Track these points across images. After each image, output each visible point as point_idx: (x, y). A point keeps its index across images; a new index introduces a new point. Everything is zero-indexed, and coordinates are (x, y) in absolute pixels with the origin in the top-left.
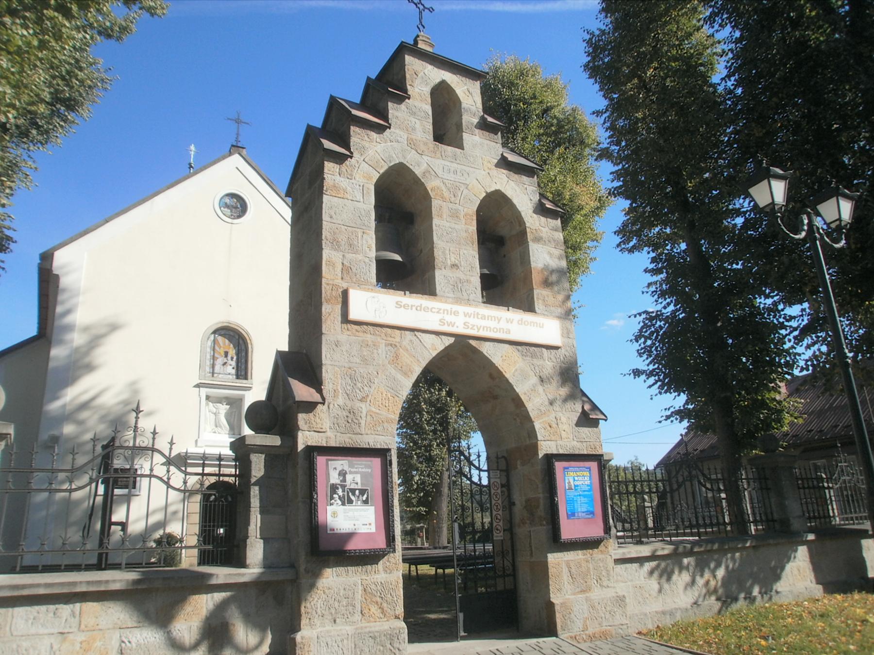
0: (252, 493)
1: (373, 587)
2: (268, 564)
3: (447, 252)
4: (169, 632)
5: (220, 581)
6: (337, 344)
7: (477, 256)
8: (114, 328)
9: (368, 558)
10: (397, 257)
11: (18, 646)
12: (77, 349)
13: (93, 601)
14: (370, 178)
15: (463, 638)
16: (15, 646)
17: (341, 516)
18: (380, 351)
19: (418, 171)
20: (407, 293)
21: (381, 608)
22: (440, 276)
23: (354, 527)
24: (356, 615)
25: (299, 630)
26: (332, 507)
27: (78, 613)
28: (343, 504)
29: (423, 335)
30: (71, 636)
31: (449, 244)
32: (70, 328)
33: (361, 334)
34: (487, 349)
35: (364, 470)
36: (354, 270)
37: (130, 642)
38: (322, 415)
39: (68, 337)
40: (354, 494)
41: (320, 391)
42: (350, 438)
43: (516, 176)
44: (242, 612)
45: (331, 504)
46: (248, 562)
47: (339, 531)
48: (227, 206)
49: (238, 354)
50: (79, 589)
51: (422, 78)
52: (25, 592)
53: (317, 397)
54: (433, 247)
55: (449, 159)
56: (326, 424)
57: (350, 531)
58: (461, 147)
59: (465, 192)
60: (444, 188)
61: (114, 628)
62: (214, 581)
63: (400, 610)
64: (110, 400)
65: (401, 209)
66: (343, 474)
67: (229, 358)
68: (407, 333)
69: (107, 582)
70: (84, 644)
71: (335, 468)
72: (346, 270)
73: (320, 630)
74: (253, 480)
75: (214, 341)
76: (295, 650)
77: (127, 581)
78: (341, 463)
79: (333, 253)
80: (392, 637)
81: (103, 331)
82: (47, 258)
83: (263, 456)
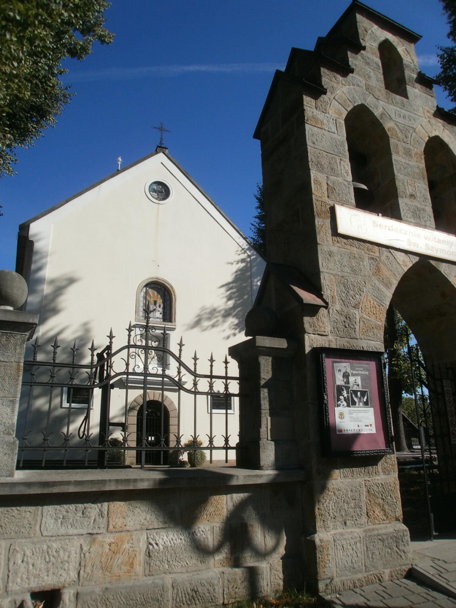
0: (262, 396)
1: (375, 488)
2: (278, 465)
3: (406, 183)
4: (194, 534)
5: (241, 482)
6: (331, 254)
7: (428, 189)
8: (71, 281)
9: (370, 460)
10: (364, 187)
11: (48, 547)
12: (46, 297)
13: (121, 501)
14: (340, 114)
15: (436, 537)
16: (45, 547)
17: (347, 416)
18: (365, 263)
19: (377, 113)
20: (380, 215)
21: (383, 510)
22: (402, 202)
23: (357, 428)
24: (363, 517)
25: (315, 532)
26: (339, 408)
27: (106, 513)
28: (348, 406)
29: (396, 252)
30: (100, 538)
31: (406, 177)
32: (41, 281)
33: (349, 247)
34: (443, 268)
35: (363, 373)
36: (337, 190)
37: (157, 544)
38: (324, 319)
39: (39, 288)
40: (356, 396)
41: (320, 295)
42: (348, 342)
43: (449, 126)
44: (258, 514)
45: (339, 406)
46: (262, 463)
47: (346, 433)
48: (154, 191)
49: (164, 302)
50: (107, 488)
51: (372, 34)
52: (56, 490)
53: (319, 302)
54: (394, 179)
55: (399, 105)
56: (328, 328)
57: (355, 432)
58: (406, 97)
59: (414, 134)
60: (397, 129)
61: (141, 529)
62: (234, 482)
63: (399, 512)
64: (69, 336)
65: (367, 141)
66: (346, 376)
67: (158, 305)
68: (384, 249)
69: (135, 480)
70: (113, 545)
71: (340, 370)
72: (331, 190)
73: (333, 532)
74: (263, 382)
75: (146, 292)
76: (315, 553)
77: (155, 480)
78: (344, 366)
79: (319, 174)
80: (397, 539)
81: (64, 283)
82: (24, 228)
83: (270, 359)
